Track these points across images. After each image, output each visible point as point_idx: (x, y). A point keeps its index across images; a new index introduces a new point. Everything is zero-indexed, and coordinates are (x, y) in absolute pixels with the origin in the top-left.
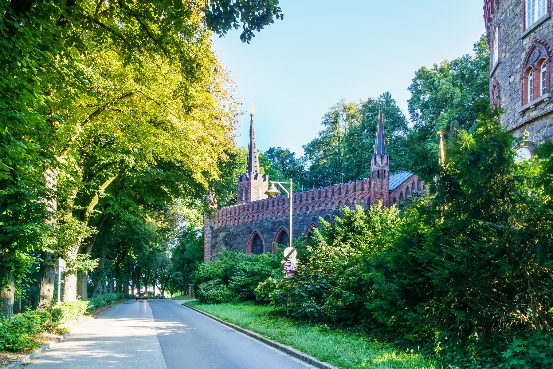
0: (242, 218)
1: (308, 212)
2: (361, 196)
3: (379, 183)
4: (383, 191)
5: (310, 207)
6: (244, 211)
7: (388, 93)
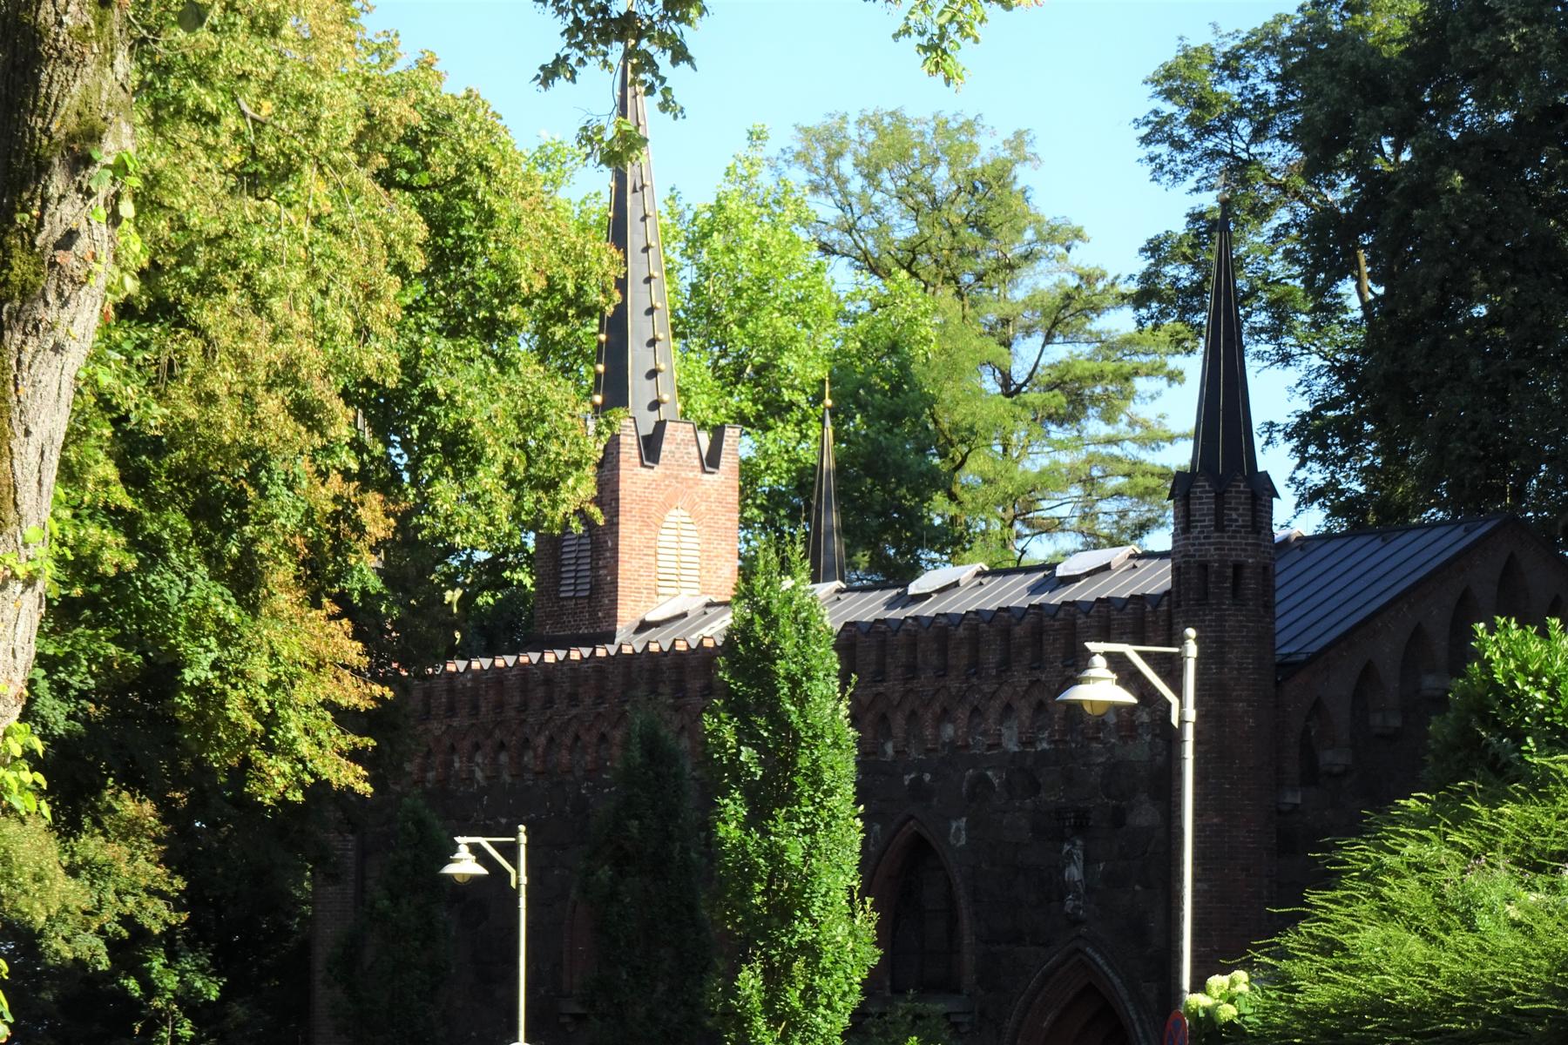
0: (542, 740)
1: (889, 748)
5: (899, 722)
6: (549, 702)
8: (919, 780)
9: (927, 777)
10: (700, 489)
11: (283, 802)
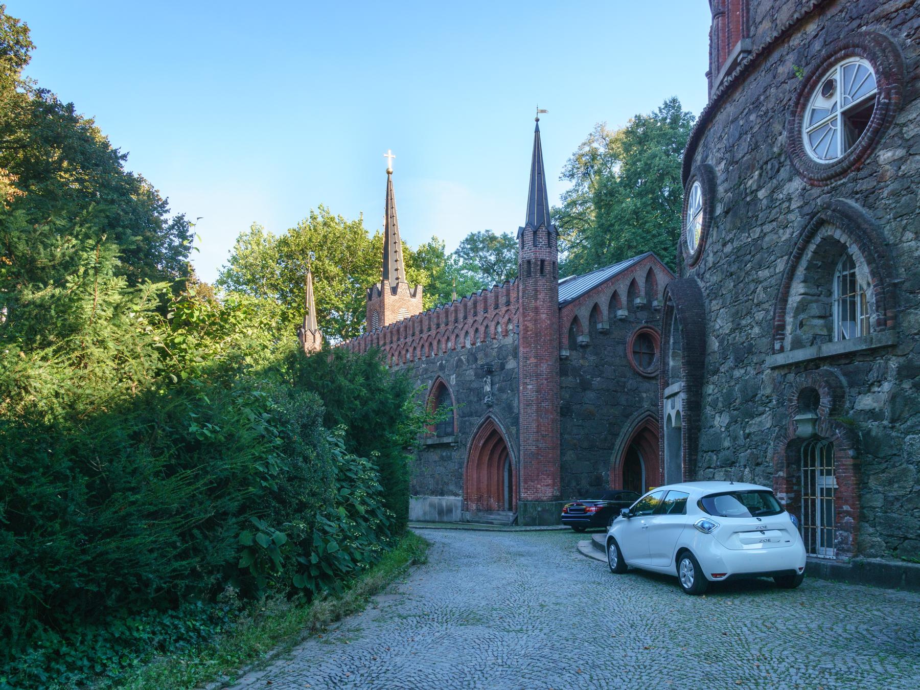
2: (507, 317)
3: (530, 288)
4: (539, 303)
5: (435, 343)
7: (674, 101)
8: (442, 363)
9: (444, 362)
10: (410, 303)
11: (19, 179)
